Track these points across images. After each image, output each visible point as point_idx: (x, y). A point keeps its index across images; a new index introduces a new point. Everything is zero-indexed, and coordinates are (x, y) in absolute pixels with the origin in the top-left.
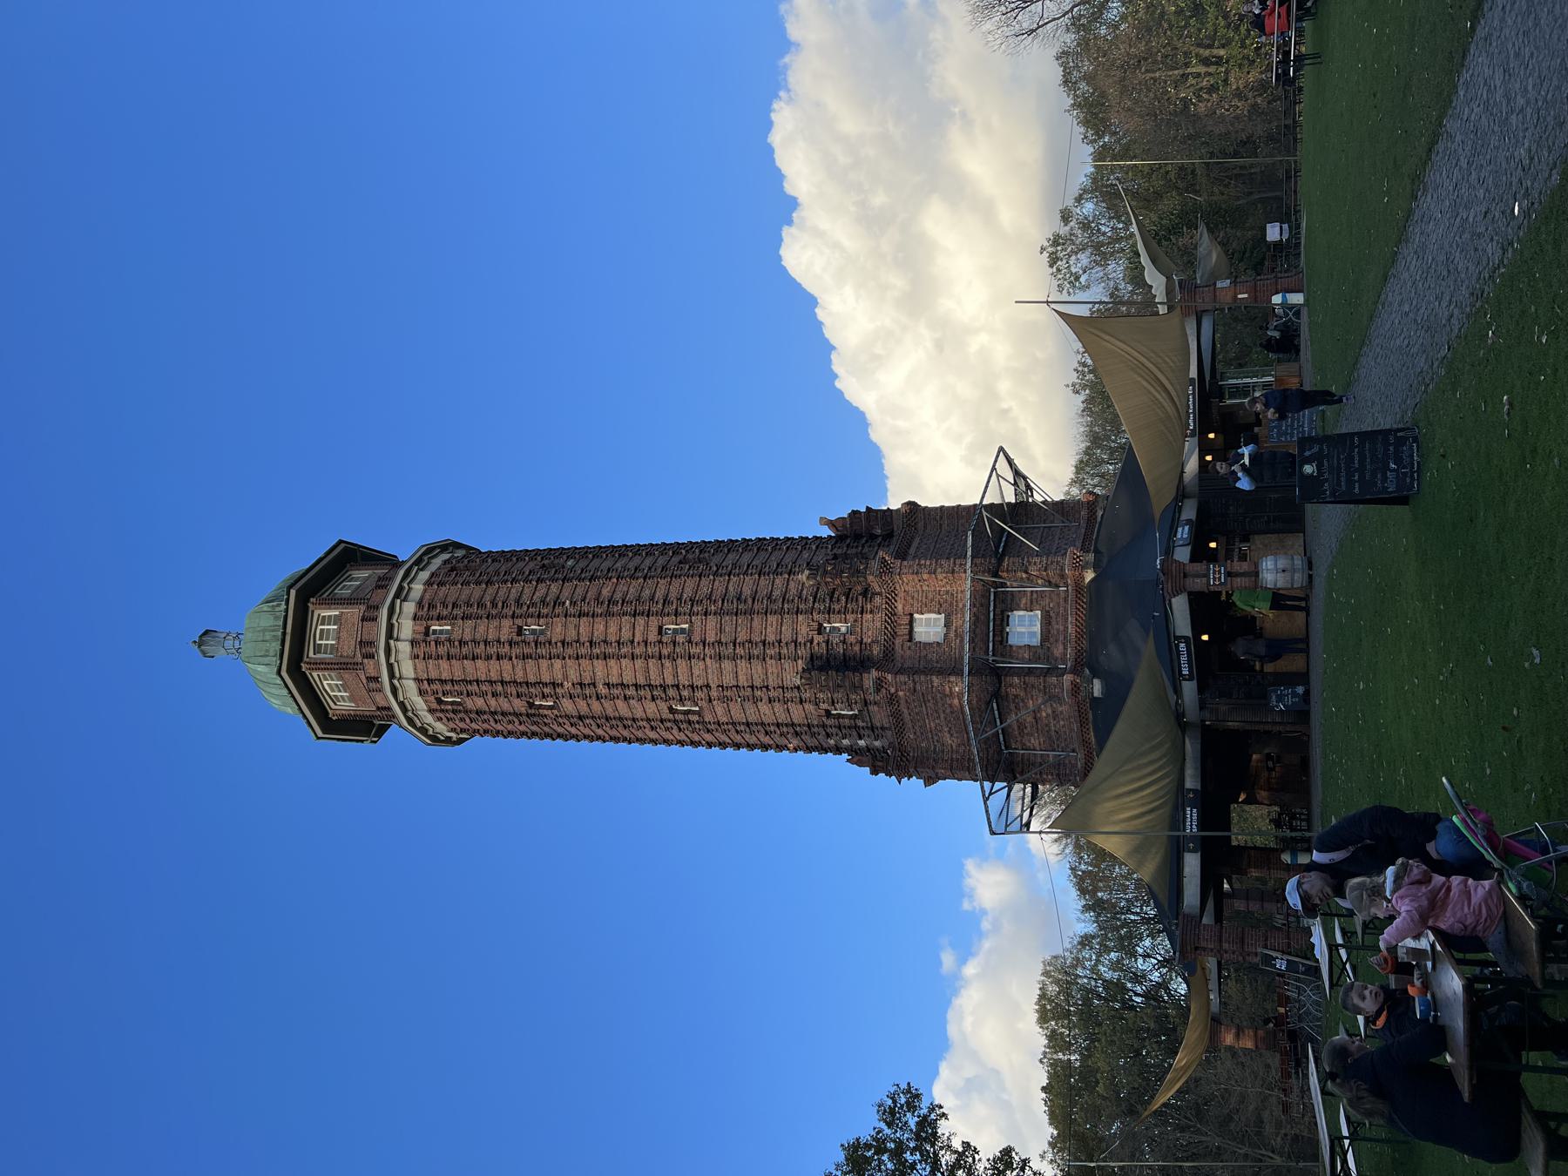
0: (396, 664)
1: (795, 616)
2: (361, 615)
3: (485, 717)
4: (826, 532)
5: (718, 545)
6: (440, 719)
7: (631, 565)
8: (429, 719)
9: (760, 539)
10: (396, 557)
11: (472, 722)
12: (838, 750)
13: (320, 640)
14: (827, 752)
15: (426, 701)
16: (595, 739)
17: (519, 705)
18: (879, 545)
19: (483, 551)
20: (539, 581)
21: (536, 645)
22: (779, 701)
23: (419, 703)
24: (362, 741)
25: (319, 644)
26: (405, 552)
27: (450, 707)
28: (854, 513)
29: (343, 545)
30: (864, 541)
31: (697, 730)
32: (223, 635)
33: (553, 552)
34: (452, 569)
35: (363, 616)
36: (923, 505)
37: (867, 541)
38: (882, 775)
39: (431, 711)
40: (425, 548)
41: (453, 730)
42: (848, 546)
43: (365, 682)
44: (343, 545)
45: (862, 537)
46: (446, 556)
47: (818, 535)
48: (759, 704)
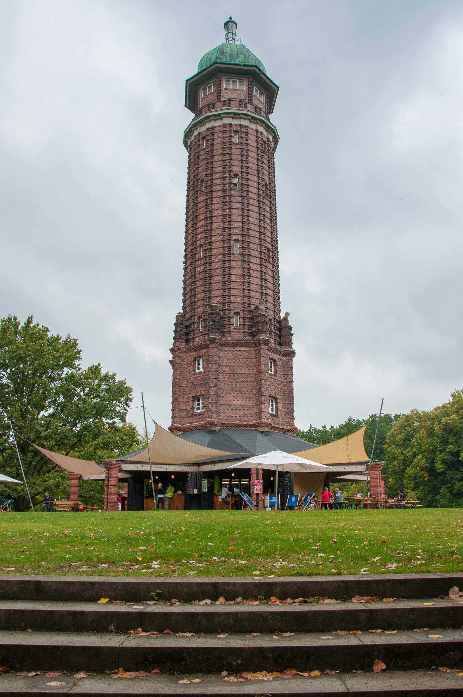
0: (220, 117)
1: (242, 331)
2: (243, 100)
3: (195, 195)
4: (282, 315)
5: (277, 266)
6: (195, 138)
7: (266, 213)
8: (196, 133)
9: (279, 285)
10: (272, 113)
11: (194, 165)
12: (184, 308)
13: (232, 81)
14: (183, 303)
15: (204, 132)
16: (189, 175)
17: (202, 175)
18: (275, 340)
19: (274, 155)
20: (259, 183)
21: (230, 148)
22: (205, 309)
23: (203, 129)
24: (184, 132)
25: (230, 81)
26: (274, 119)
27: (202, 198)
28: (291, 328)
29: (277, 89)
30: (277, 332)
31: (191, 271)
32: (234, 33)
33: (273, 188)
34: (265, 142)
35: (242, 101)
36: (294, 359)
37: (277, 334)
38: (174, 335)
39: (199, 134)
40: (274, 129)
41: (191, 143)
42: (275, 325)
43: (213, 102)
44: (277, 89)
45: (280, 332)
46: (271, 138)
47: (279, 266)
48: (205, 208)
